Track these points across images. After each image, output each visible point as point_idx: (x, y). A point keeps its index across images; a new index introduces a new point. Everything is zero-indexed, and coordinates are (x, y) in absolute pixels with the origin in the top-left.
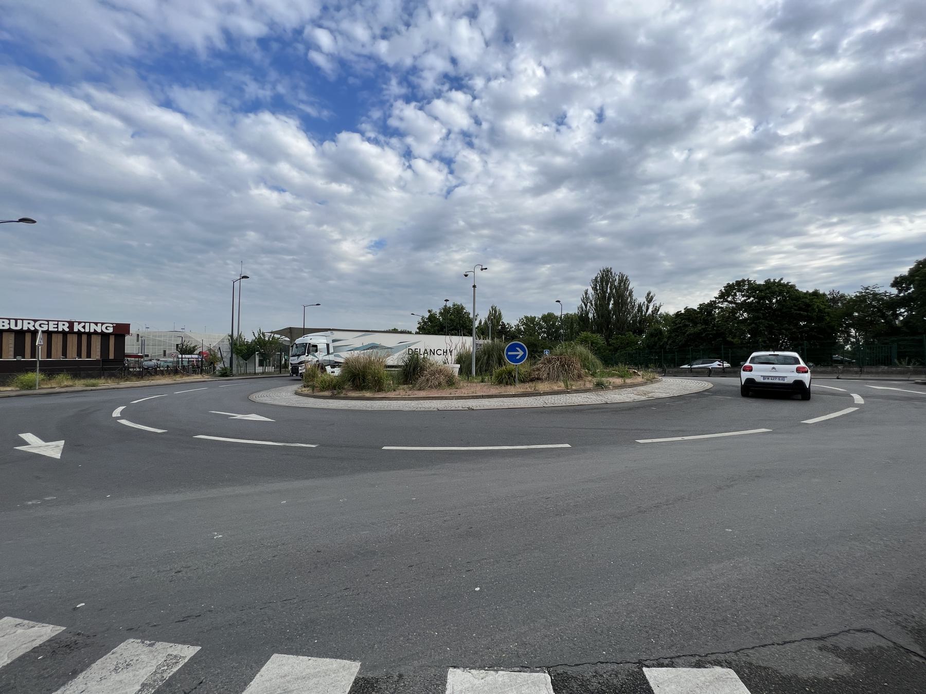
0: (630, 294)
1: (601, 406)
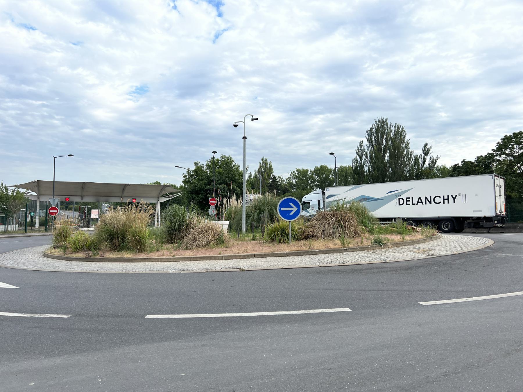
0: (407, 146)
1: (380, 265)
